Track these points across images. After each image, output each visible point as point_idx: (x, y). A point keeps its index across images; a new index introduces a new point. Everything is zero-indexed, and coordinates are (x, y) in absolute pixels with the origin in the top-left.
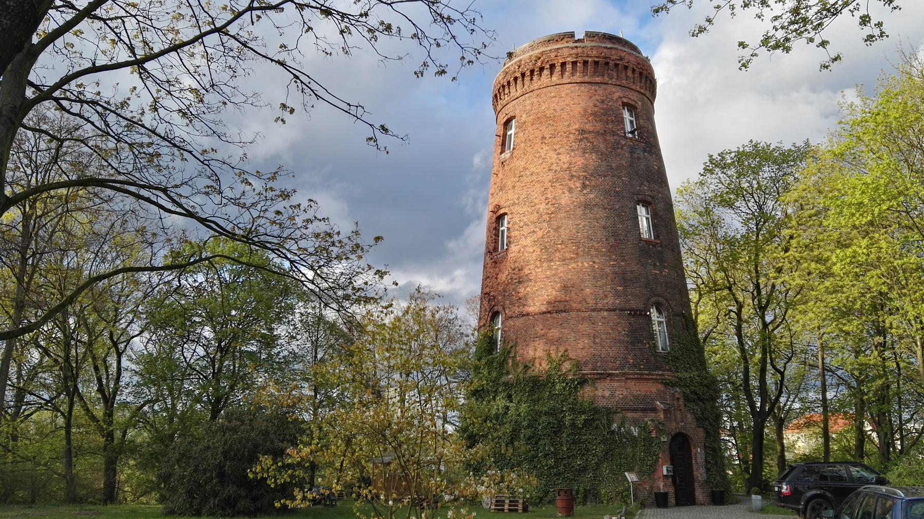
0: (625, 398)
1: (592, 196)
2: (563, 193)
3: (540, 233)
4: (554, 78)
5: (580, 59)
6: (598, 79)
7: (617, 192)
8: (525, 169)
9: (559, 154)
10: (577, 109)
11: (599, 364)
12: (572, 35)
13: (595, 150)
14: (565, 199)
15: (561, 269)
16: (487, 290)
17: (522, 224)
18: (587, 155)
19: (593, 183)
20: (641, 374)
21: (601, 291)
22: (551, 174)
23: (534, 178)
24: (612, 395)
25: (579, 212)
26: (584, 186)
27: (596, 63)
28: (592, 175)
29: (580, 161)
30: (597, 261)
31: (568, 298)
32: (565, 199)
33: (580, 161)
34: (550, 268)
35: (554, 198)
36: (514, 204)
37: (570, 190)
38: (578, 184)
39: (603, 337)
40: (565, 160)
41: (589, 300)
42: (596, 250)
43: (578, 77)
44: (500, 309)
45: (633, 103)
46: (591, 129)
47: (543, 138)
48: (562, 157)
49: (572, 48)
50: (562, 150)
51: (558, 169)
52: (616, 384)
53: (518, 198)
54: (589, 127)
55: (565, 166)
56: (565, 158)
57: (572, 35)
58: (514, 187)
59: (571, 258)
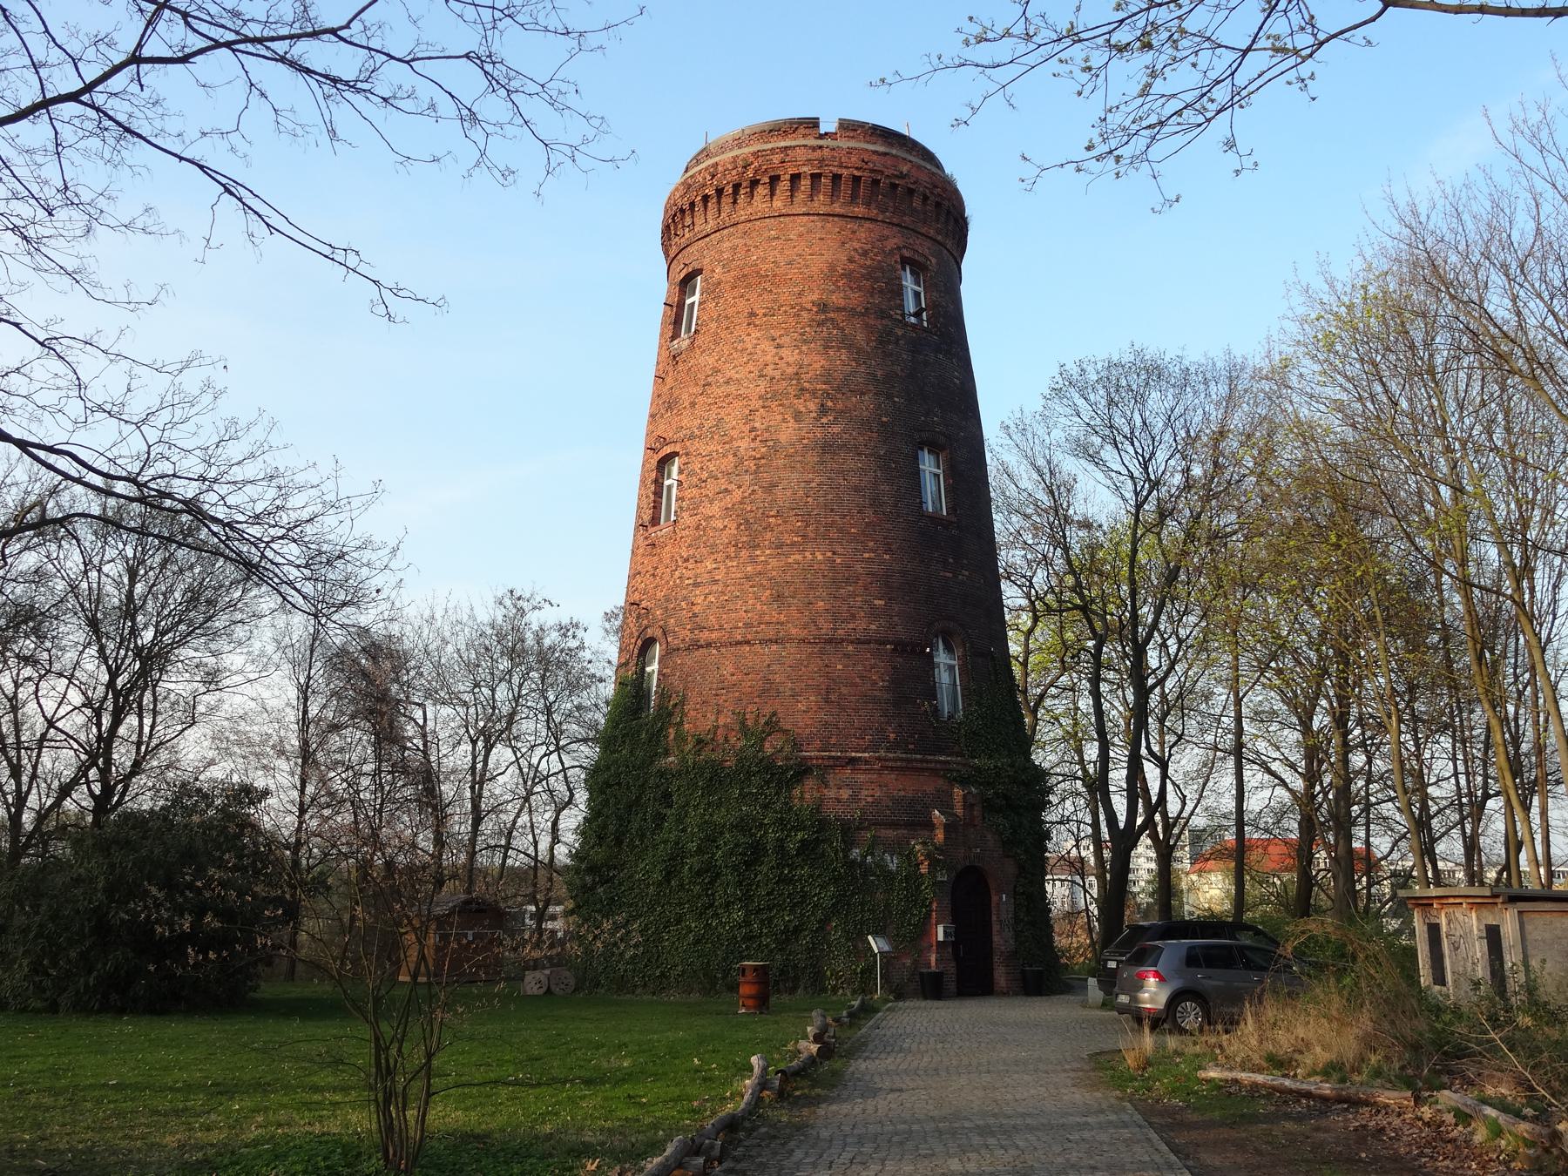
0: (877, 802)
1: (836, 429)
2: (784, 420)
3: (737, 495)
4: (742, 214)
5: (845, 172)
6: (859, 210)
7: (883, 424)
8: (716, 371)
9: (779, 346)
10: (818, 265)
11: (833, 740)
12: (813, 123)
13: (846, 343)
14: (788, 433)
15: (774, 562)
16: (636, 597)
17: (705, 475)
18: (831, 352)
19: (840, 406)
20: (907, 760)
21: (845, 607)
22: (763, 383)
23: (732, 388)
24: (855, 798)
25: (812, 458)
26: (823, 410)
27: (856, 179)
28: (838, 390)
29: (818, 363)
30: (839, 549)
31: (783, 618)
32: (788, 433)
33: (818, 363)
34: (753, 560)
35: (767, 430)
36: (692, 437)
37: (798, 416)
38: (812, 406)
39: (844, 690)
40: (791, 360)
41: (821, 622)
42: (840, 530)
43: (821, 203)
44: (658, 633)
45: (921, 259)
46: (842, 303)
47: (752, 314)
48: (784, 352)
49: (814, 149)
50: (786, 340)
51: (777, 374)
52: (862, 777)
53: (701, 426)
54: (836, 299)
55: (790, 370)
56: (790, 355)
57: (813, 123)
58: (693, 404)
59: (793, 544)
